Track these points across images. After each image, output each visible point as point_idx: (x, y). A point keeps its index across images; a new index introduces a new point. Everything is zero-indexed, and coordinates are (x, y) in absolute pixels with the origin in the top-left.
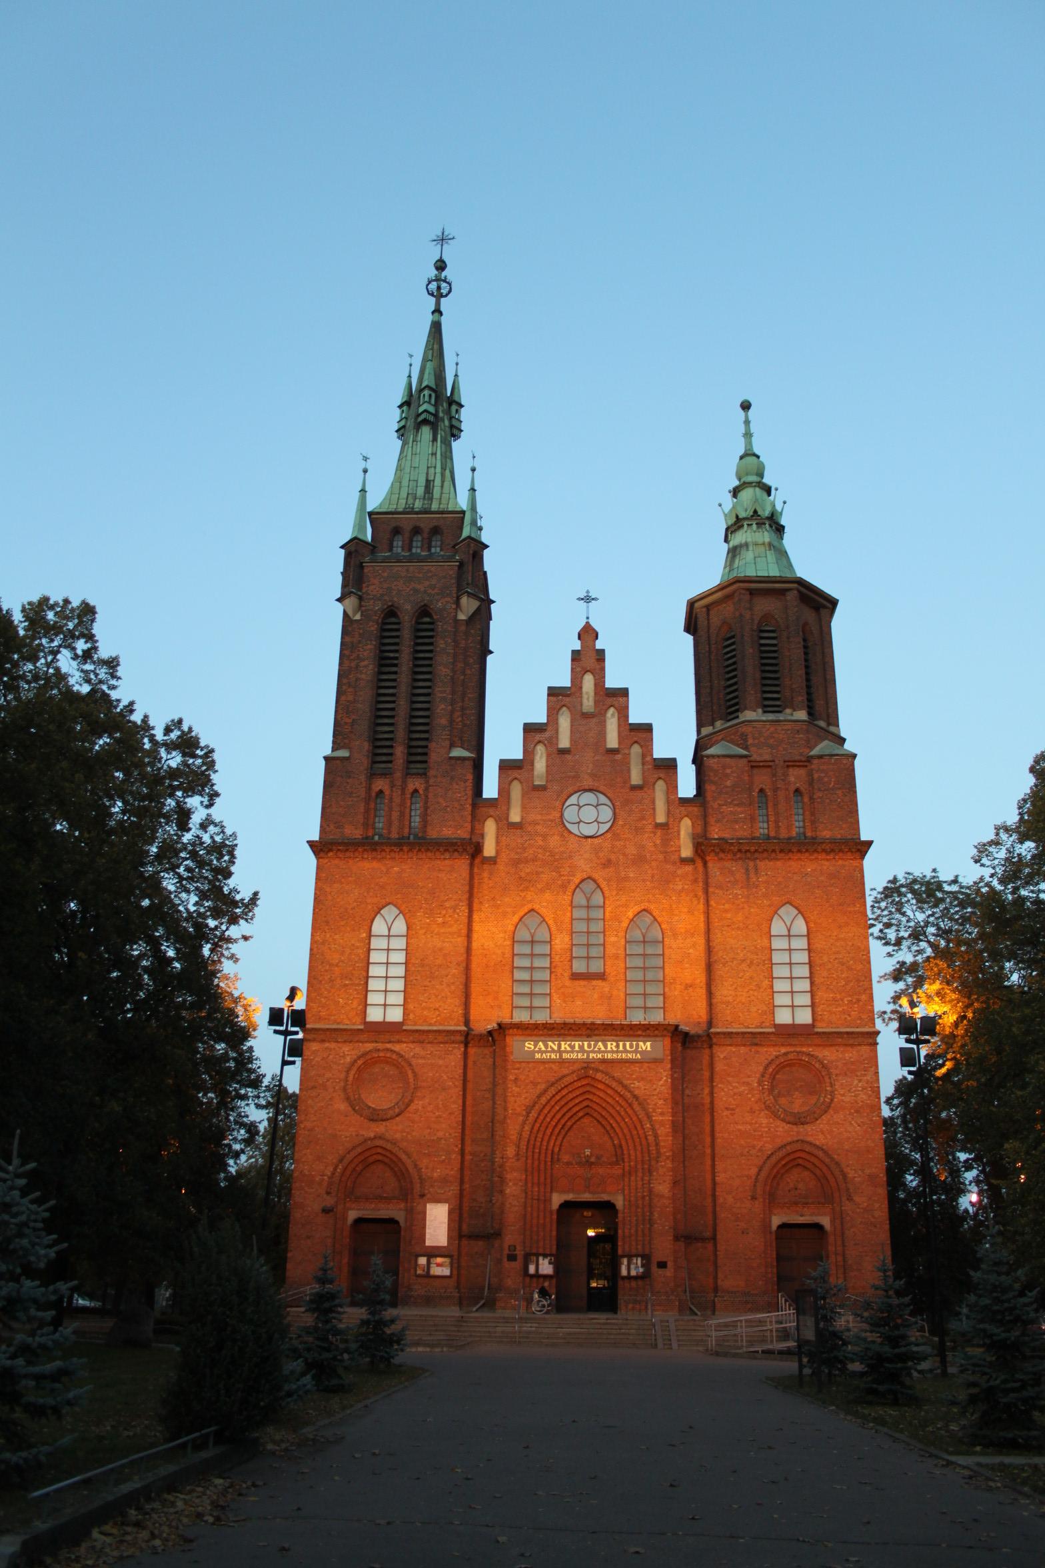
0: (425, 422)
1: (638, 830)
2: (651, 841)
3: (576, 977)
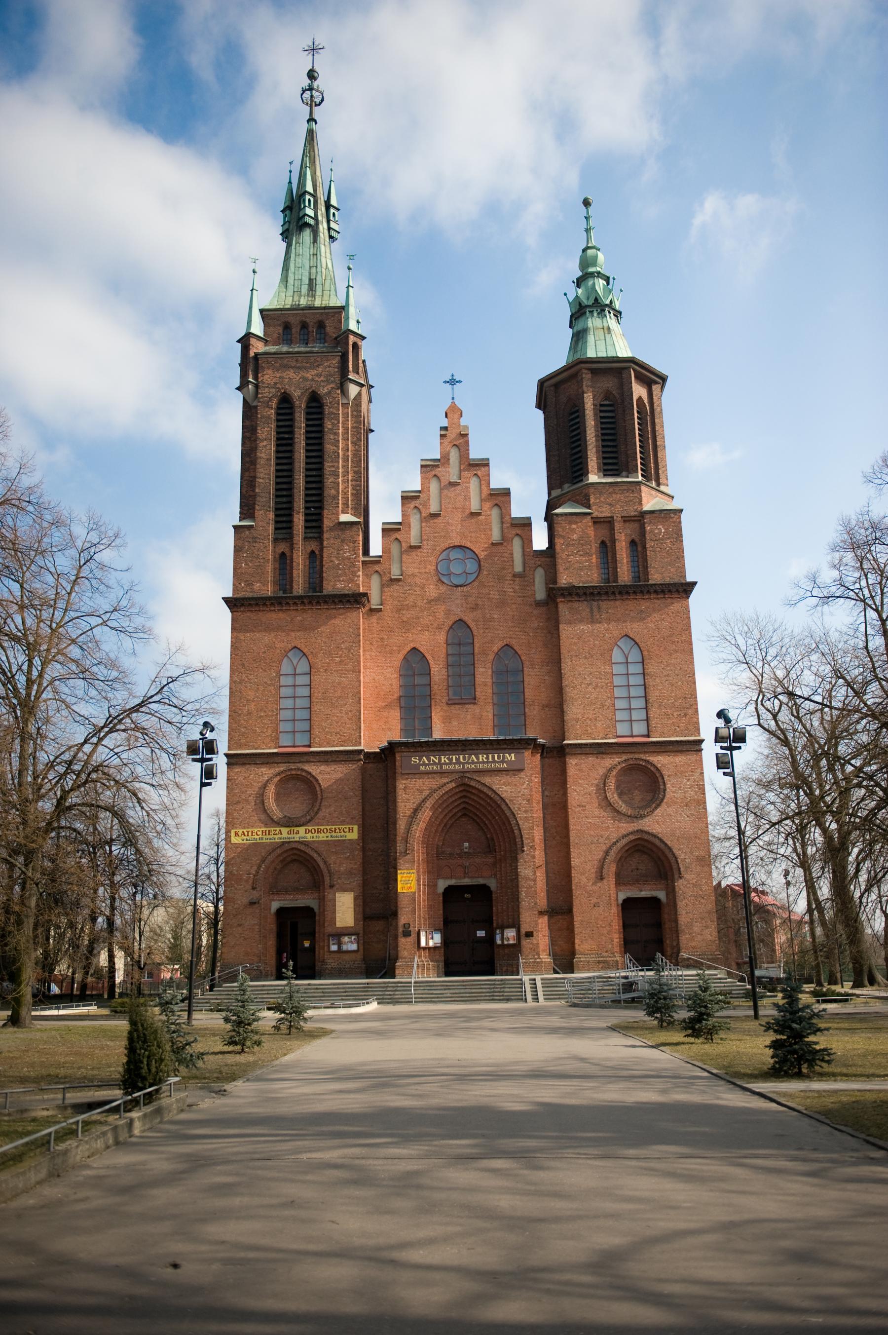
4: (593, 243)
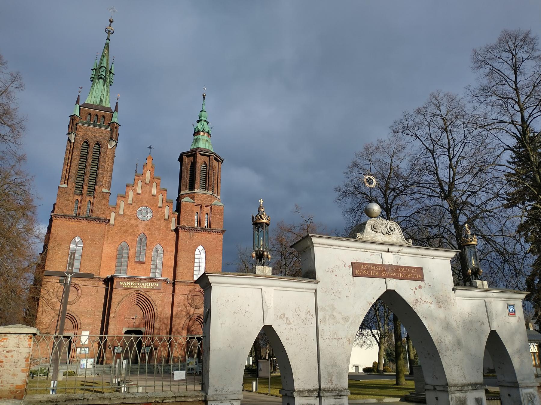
0: (102, 78)
1: (160, 220)
2: (163, 224)
3: (136, 262)
4: (204, 109)
